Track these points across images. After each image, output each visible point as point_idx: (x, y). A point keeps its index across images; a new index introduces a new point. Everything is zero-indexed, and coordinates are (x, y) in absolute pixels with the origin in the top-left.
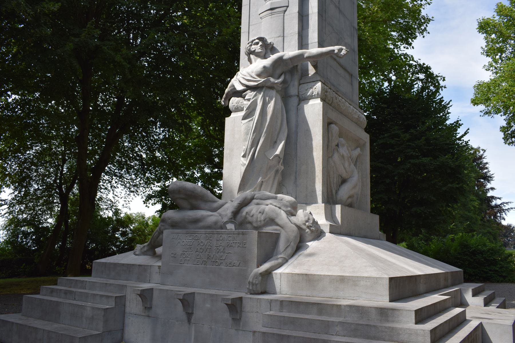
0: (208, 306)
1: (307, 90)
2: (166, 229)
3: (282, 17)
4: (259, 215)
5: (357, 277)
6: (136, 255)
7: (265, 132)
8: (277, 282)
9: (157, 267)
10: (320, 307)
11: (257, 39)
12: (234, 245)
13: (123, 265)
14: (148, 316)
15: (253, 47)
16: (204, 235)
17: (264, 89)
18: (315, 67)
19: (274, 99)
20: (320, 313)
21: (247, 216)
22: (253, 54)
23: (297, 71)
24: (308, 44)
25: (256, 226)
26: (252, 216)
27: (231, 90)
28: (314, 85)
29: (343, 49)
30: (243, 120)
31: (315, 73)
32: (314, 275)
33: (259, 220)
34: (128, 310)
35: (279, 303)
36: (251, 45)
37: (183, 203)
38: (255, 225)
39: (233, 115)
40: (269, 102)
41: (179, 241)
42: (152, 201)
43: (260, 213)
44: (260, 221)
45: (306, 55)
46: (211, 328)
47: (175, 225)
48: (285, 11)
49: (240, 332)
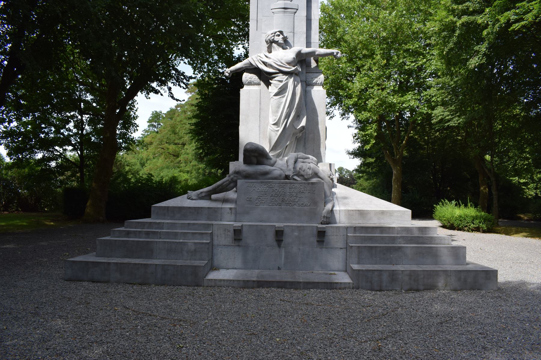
0: (296, 234)
1: (313, 78)
6: (192, 199)
8: (337, 216)
10: (382, 229)
11: (279, 31)
12: (305, 192)
13: (190, 208)
14: (239, 246)
15: (276, 38)
17: (294, 75)
23: (402, 96)
24: (311, 43)
28: (318, 76)
30: (274, 96)
34: (216, 242)
35: (353, 229)
36: (274, 36)
37: (254, 160)
38: (306, 177)
39: (245, 87)
40: (297, 86)
42: (272, 162)
45: (317, 53)
46: (299, 249)
47: (247, 176)
48: (295, 13)
49: (324, 249)
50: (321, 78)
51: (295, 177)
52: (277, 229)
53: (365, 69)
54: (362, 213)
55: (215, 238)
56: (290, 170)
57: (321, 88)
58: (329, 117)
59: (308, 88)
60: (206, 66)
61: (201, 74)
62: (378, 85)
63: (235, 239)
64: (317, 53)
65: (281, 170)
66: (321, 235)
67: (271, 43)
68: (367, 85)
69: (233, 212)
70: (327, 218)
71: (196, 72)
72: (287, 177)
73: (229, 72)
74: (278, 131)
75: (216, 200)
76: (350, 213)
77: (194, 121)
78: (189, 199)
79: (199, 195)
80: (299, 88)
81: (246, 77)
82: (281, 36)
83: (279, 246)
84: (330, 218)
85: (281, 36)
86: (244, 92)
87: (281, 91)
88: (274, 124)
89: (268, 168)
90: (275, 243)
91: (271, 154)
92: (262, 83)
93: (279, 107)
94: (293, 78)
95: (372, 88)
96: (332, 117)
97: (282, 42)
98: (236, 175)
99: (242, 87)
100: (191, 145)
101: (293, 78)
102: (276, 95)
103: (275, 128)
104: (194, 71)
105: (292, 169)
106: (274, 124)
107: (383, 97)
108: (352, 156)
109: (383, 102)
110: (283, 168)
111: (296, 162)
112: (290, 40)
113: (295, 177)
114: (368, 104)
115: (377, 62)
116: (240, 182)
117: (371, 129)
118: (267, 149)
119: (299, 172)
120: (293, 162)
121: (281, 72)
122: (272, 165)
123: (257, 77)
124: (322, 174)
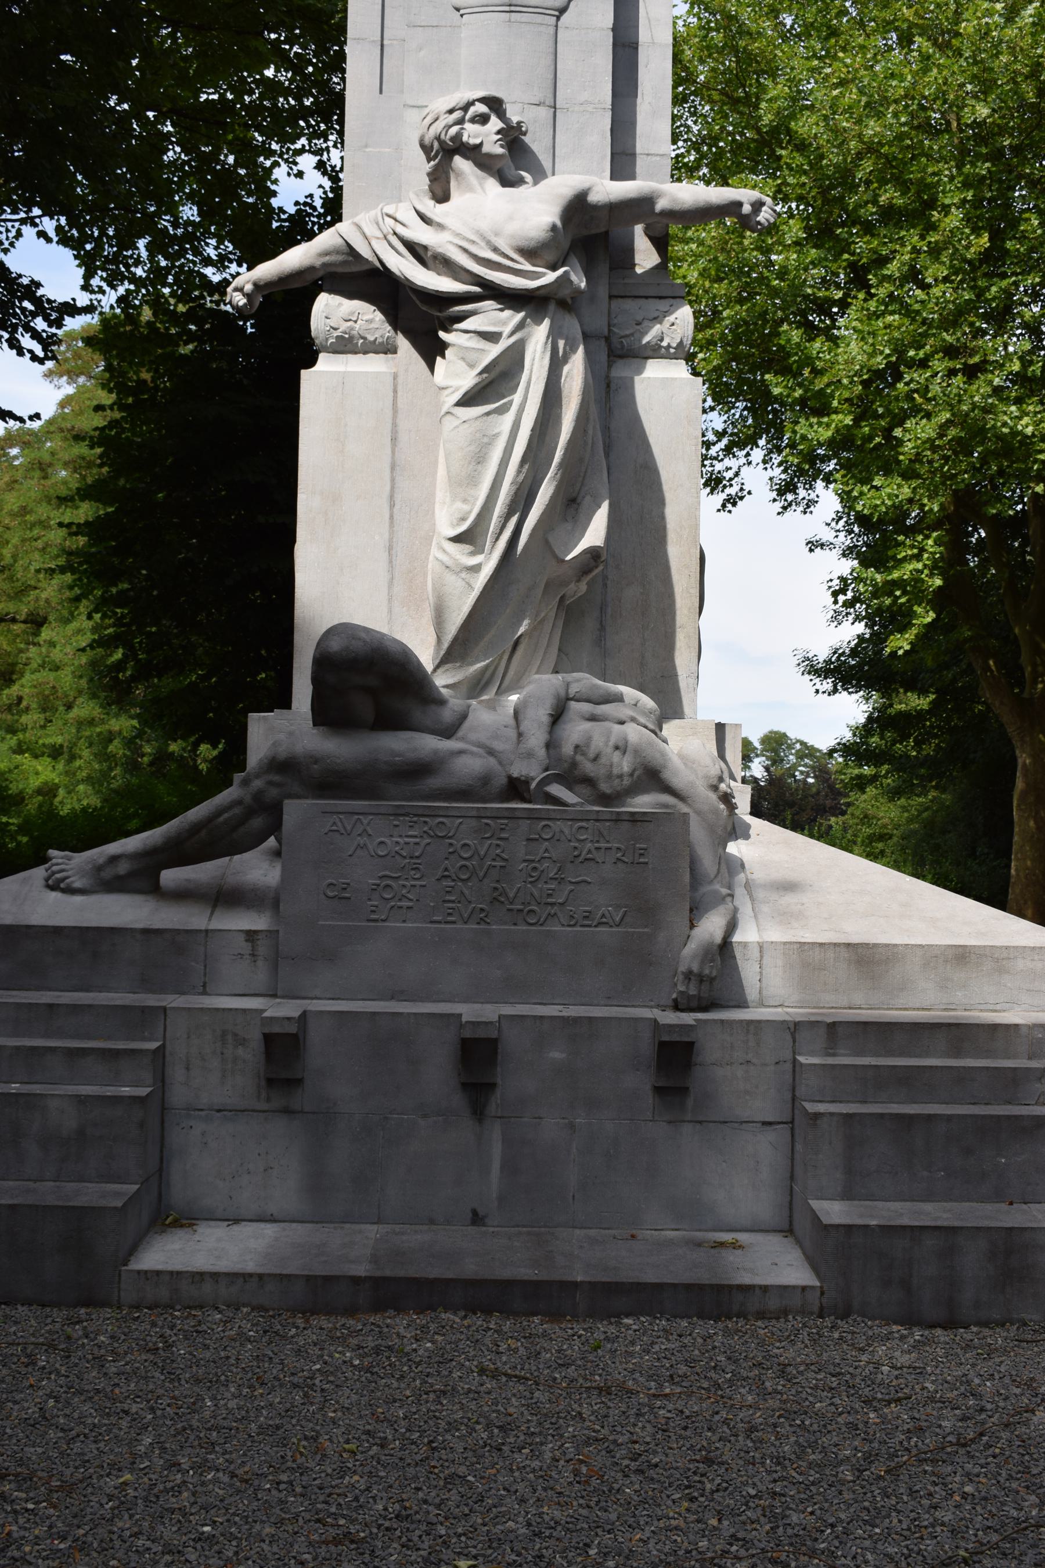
0: (557, 1055)
2: (290, 796)
3: (552, 30)
4: (616, 756)
5: (1007, 948)
7: (561, 465)
9: (242, 937)
10: (960, 1035)
11: (483, 100)
12: (599, 856)
13: (58, 931)
14: (287, 1111)
15: (472, 134)
16: (474, 823)
17: (552, 307)
18: (661, 243)
19: (561, 354)
20: (958, 1052)
21: (579, 758)
22: (466, 157)
24: (633, 155)
25: (608, 791)
26: (596, 759)
27: (324, 265)
28: (667, 313)
29: (763, 204)
31: (656, 268)
32: (875, 945)
33: (615, 771)
34: (178, 1095)
36: (461, 121)
38: (604, 787)
39: (325, 363)
40: (566, 359)
41: (361, 841)
42: (447, 715)
43: (617, 748)
44: (620, 776)
45: (661, 205)
46: (572, 1126)
50: (681, 322)
51: (557, 790)
52: (467, 1034)
53: (889, 278)
54: (866, 959)
55: (177, 1074)
56: (530, 755)
57: (680, 370)
58: (719, 498)
59: (619, 371)
60: (144, 254)
61: (121, 290)
62: (950, 352)
63: (270, 1082)
64: (661, 205)
65: (491, 752)
66: (675, 1062)
67: (444, 154)
68: (899, 350)
69: (262, 949)
70: (701, 979)
71: (95, 282)
72: (516, 788)
73: (248, 288)
74: (476, 569)
75: (182, 895)
76: (808, 958)
77: (85, 512)
78: (52, 888)
79: (99, 868)
80: (575, 372)
81: (330, 312)
82: (495, 124)
83: (478, 1112)
84: (715, 979)
85: (495, 124)
86: (320, 384)
87: (493, 385)
88: (457, 539)
89: (429, 744)
90: (458, 1100)
91: (441, 680)
92: (403, 343)
93: (480, 459)
94: (546, 323)
95: (923, 364)
96: (733, 500)
97: (499, 150)
98: (277, 778)
99: (311, 362)
100: (74, 625)
101: (546, 323)
102: (468, 400)
103: (461, 554)
104: (88, 276)
105: (542, 752)
106: (457, 539)
107: (974, 406)
108: (828, 685)
109: (971, 432)
110: (498, 746)
111: (558, 716)
112: (536, 141)
113: (557, 790)
114: (900, 442)
115: (948, 242)
116: (294, 811)
117: (918, 557)
118: (426, 656)
119: (574, 764)
120: (546, 719)
121: (492, 292)
122: (448, 732)
123: (379, 316)
124: (680, 775)
